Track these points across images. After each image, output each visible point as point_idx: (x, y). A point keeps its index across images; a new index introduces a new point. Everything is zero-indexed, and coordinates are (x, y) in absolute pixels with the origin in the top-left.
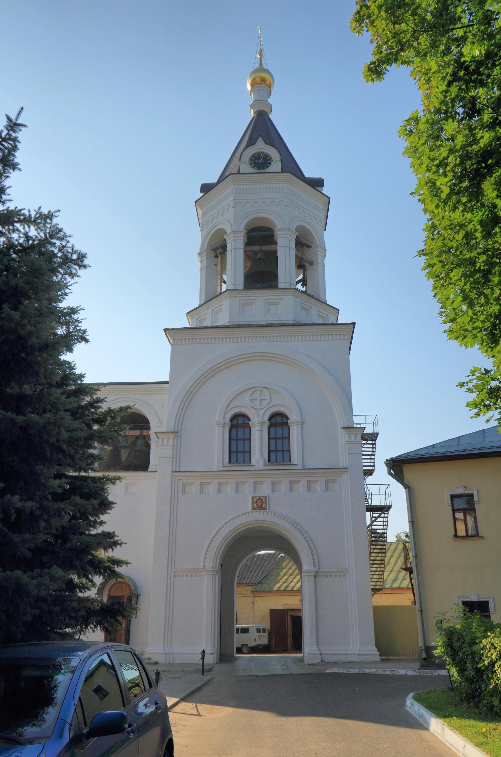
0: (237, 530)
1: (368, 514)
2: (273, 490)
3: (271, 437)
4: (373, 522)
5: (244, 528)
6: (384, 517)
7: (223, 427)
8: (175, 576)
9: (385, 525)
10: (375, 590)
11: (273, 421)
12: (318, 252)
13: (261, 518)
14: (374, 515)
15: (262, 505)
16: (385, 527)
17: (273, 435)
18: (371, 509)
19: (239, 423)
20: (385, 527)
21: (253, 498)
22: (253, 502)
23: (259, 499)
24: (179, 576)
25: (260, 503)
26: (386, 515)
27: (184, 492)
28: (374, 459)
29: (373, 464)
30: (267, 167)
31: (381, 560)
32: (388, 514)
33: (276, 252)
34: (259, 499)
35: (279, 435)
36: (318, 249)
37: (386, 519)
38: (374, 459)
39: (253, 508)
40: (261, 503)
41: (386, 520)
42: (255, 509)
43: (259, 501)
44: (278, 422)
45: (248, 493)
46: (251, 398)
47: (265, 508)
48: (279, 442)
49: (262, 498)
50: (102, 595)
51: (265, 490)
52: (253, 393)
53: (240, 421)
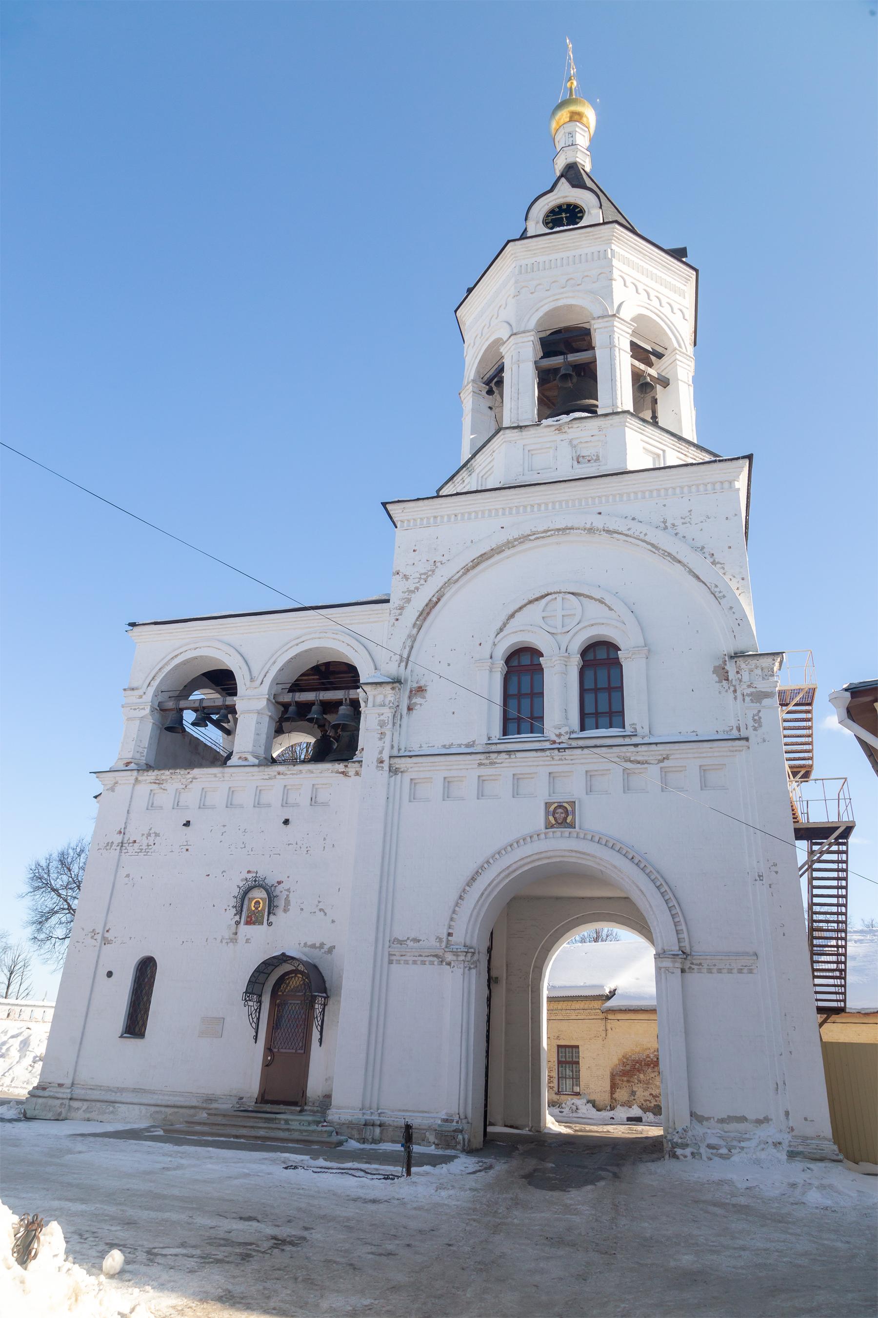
0: (515, 871)
1: (802, 846)
2: (589, 790)
3: (586, 711)
4: (813, 862)
5: (529, 866)
6: (838, 852)
7: (491, 671)
8: (390, 962)
9: (842, 896)
10: (828, 1013)
11: (590, 656)
12: (678, 362)
13: (561, 846)
14: (815, 848)
15: (565, 819)
16: (841, 901)
17: (589, 684)
18: (806, 833)
19: (522, 668)
20: (841, 901)
21: (547, 805)
22: (547, 813)
23: (560, 806)
24: (398, 962)
25: (561, 816)
26: (844, 848)
27: (413, 798)
28: (809, 728)
29: (810, 755)
30: (581, 218)
31: (838, 879)
32: (845, 844)
33: (594, 361)
34: (560, 806)
35: (602, 683)
36: (678, 357)
37: (844, 856)
38: (809, 728)
39: (549, 826)
40: (563, 815)
41: (844, 893)
42: (552, 827)
43: (560, 810)
44: (601, 664)
45: (539, 794)
46: (544, 614)
47: (572, 826)
48: (603, 697)
49: (565, 805)
50: (260, 996)
51: (572, 788)
52: (547, 604)
53: (526, 660)
